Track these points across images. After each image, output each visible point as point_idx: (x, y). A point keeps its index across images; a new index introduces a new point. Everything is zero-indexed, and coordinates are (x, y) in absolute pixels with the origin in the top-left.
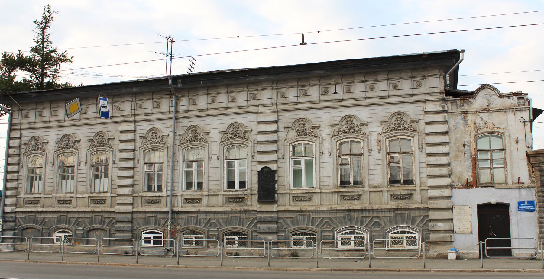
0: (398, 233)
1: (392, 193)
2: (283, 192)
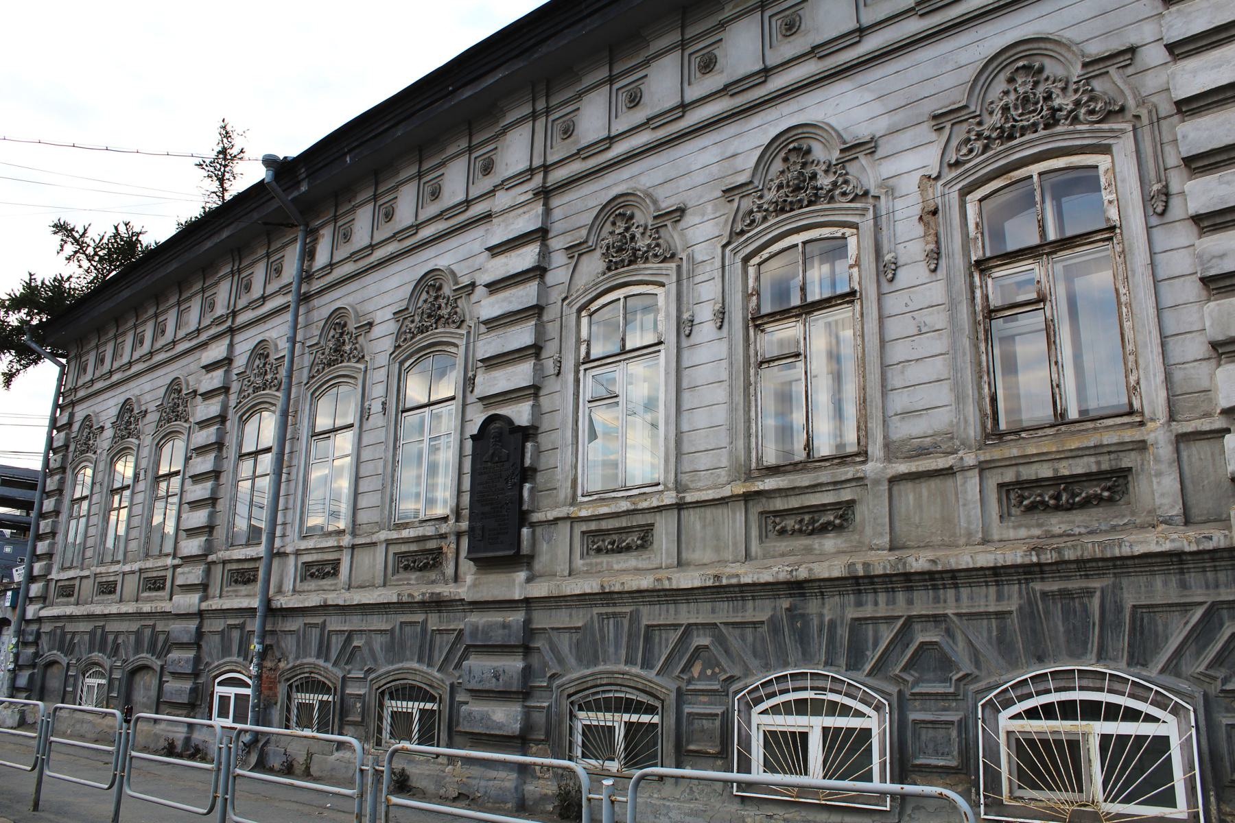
0: (1048, 711)
1: (1009, 476)
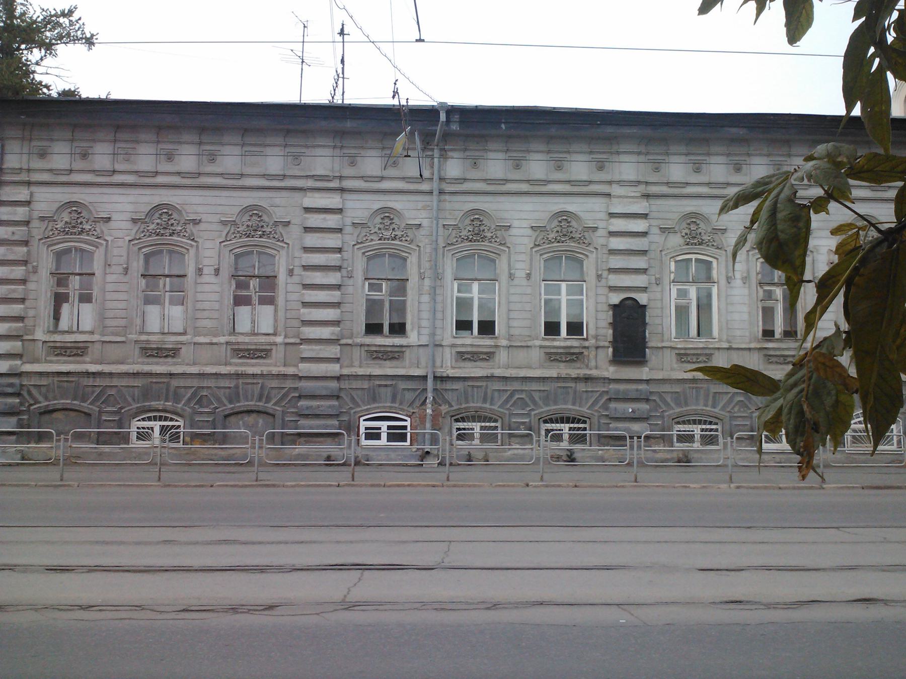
2: (660, 345)
